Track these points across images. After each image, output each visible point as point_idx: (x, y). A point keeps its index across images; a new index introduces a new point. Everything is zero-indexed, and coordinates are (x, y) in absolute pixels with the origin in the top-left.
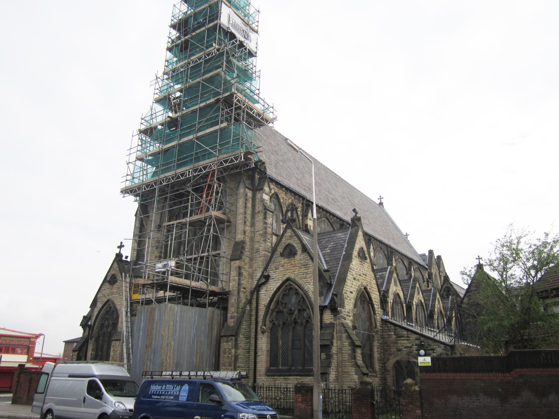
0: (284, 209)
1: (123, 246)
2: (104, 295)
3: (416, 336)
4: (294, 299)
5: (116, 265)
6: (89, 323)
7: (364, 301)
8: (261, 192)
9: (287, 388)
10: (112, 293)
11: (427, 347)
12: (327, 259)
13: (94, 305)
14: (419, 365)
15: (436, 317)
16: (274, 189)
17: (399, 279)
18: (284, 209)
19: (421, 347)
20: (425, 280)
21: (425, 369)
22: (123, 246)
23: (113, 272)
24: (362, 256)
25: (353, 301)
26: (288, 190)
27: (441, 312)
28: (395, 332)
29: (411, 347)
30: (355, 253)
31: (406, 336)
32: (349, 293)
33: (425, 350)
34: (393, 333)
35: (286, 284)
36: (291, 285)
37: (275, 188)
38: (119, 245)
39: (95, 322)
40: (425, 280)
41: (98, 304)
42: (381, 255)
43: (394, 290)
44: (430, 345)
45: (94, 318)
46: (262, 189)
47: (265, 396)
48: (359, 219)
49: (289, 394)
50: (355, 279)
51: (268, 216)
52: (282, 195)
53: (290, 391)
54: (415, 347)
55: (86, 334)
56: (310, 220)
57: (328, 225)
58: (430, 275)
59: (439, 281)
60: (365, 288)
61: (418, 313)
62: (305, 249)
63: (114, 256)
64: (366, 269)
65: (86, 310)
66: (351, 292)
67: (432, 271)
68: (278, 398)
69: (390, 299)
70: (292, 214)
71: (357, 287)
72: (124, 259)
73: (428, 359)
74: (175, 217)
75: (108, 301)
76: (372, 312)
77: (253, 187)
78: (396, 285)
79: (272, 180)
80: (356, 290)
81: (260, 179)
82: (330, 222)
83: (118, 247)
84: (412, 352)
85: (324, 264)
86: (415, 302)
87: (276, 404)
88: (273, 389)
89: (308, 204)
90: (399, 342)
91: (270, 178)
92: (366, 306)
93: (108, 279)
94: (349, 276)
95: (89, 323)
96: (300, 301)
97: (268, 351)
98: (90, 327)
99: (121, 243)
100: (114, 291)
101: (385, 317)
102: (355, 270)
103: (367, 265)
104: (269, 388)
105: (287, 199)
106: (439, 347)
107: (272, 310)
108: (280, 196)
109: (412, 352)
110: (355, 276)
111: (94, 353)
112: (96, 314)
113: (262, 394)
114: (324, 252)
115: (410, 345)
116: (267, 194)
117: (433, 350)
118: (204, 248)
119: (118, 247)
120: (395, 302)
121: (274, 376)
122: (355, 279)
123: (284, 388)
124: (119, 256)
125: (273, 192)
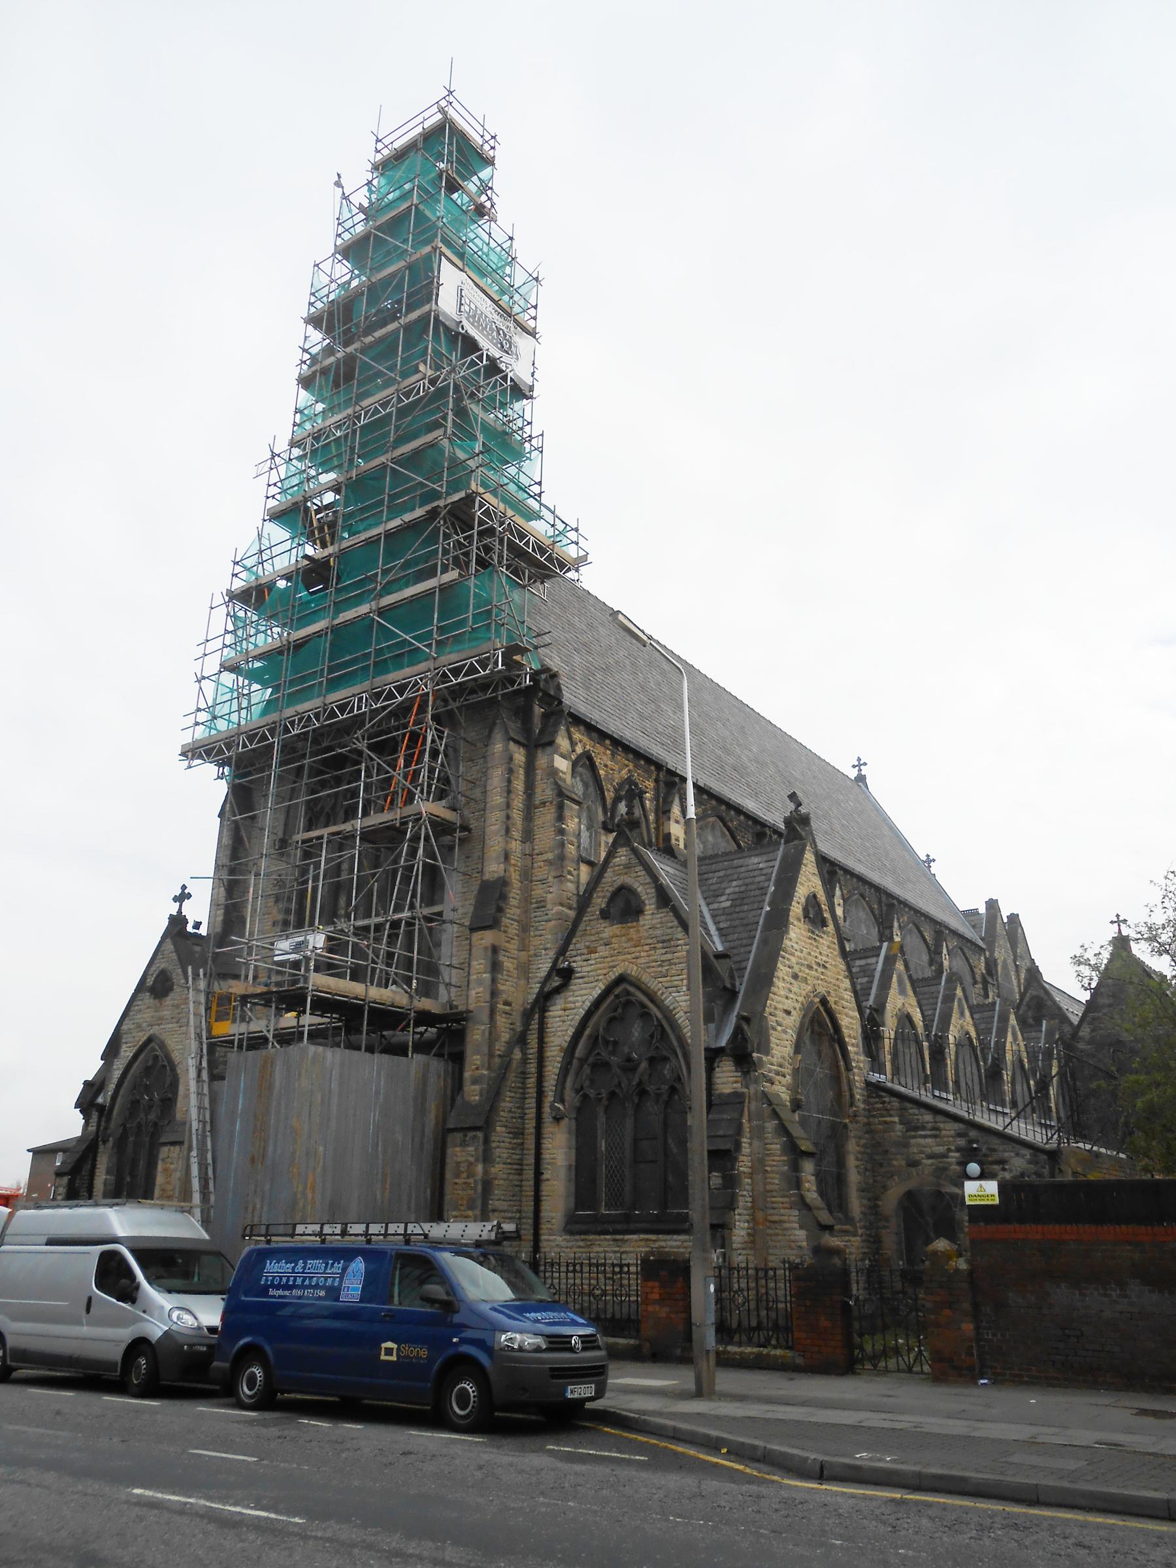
0: (610, 796)
1: (189, 896)
2: (139, 1026)
3: (962, 1126)
5: (169, 946)
6: (100, 1100)
7: (820, 1034)
8: (549, 750)
9: (621, 1266)
10: (161, 1018)
11: (985, 1155)
12: (722, 925)
13: (111, 1052)
14: (968, 1202)
15: (1006, 1076)
16: (584, 743)
17: (910, 977)
18: (610, 796)
19: (970, 1154)
20: (979, 978)
21: (981, 1213)
22: (189, 896)
23: (161, 965)
24: (815, 917)
25: (791, 1035)
26: (619, 745)
27: (1021, 1061)
29: (945, 1156)
30: (796, 909)
32: (781, 1014)
33: (980, 1163)
34: (896, 1119)
35: (617, 991)
36: (628, 993)
37: (585, 739)
38: (178, 892)
39: (114, 1098)
40: (979, 978)
42: (862, 914)
43: (899, 1005)
44: (994, 1150)
45: (111, 1087)
46: (551, 743)
48: (805, 820)
50: (795, 976)
51: (567, 813)
52: (603, 758)
53: (628, 1272)
55: (92, 1128)
56: (677, 822)
57: (723, 835)
59: (1015, 982)
60: (824, 1002)
62: (664, 899)
63: (165, 923)
64: (825, 950)
65: (91, 1067)
66: (788, 1013)
67: (996, 954)
69: (889, 1030)
70: (630, 807)
71: (800, 999)
72: (190, 928)
73: (991, 1187)
75: (150, 1040)
77: (528, 738)
78: (903, 992)
79: (577, 720)
80: (798, 1006)
81: (546, 716)
82: (729, 829)
83: (175, 899)
84: (945, 1169)
85: (716, 939)
86: (953, 1035)
88: (586, 1269)
89: (671, 782)
90: (913, 1141)
91: (571, 715)
92: (825, 1048)
93: (150, 982)
94: (782, 971)
95: (100, 1100)
98: (101, 1109)
99: (184, 887)
100: (166, 1013)
101: (876, 1077)
102: (797, 953)
103: (827, 943)
104: (574, 1267)
105: (616, 767)
107: (580, 1059)
108: (597, 761)
109: (945, 1169)
110: (796, 969)
111: (111, 1178)
112: (117, 1074)
114: (715, 906)
116: (563, 756)
117: (1002, 1162)
118: (402, 897)
119: (175, 899)
120: (899, 1037)
121: (586, 1233)
124: (177, 921)
125: (579, 749)
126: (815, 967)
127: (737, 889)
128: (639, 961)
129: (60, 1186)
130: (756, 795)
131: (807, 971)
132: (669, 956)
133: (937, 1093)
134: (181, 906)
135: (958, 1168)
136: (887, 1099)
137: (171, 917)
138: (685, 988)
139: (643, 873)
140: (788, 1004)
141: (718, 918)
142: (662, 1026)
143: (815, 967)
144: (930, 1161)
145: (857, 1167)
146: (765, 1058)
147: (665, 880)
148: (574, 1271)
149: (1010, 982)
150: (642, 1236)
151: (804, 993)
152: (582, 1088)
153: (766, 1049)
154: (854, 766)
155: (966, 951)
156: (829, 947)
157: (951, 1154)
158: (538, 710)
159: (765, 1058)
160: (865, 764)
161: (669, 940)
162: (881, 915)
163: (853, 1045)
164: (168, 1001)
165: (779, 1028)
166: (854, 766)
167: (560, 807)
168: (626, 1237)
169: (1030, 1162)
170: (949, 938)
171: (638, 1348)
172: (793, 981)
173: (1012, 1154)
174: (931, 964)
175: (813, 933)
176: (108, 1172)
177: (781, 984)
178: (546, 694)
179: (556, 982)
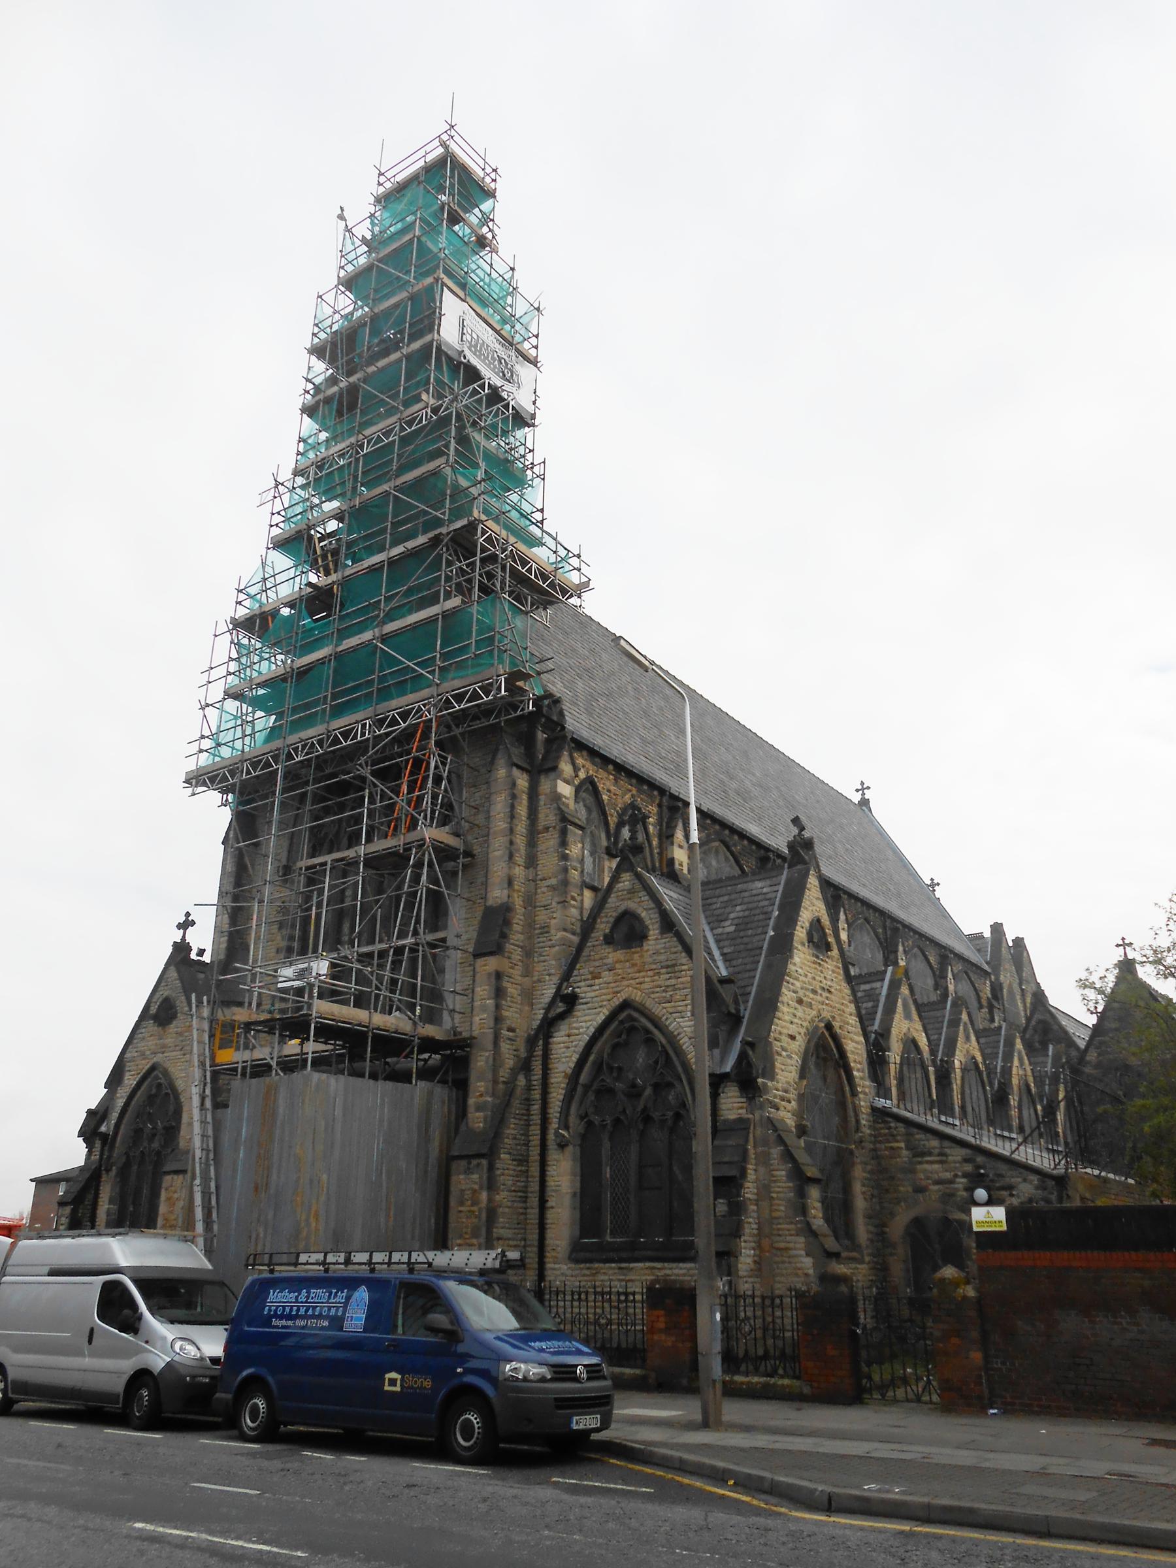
0: (613, 821)
1: (193, 923)
2: (143, 1054)
3: (968, 1151)
4: (641, 1058)
5: (173, 974)
6: (103, 1129)
8: (552, 775)
10: (164, 1046)
11: (992, 1181)
12: (726, 950)
13: (115, 1079)
14: (975, 1229)
15: (1013, 1101)
16: (587, 768)
17: (915, 1001)
18: (613, 821)
19: (977, 1180)
20: (984, 1003)
21: (988, 1239)
22: (193, 923)
23: (165, 992)
24: (819, 941)
25: (797, 1060)
26: (622, 770)
27: (1028, 1086)
28: (907, 1142)
29: (951, 1182)
30: (800, 933)
31: (936, 1151)
32: (785, 1039)
34: (902, 1145)
35: (622, 1016)
38: (182, 919)
40: (984, 1003)
41: (127, 1076)
43: (905, 1030)
44: (1001, 1176)
46: (554, 768)
47: (568, 1315)
48: (808, 845)
49: (631, 1311)
50: (800, 1001)
52: (606, 782)
53: (634, 1301)
54: (962, 1182)
55: (96, 1157)
56: (680, 847)
57: (727, 859)
58: (996, 989)
60: (829, 1027)
61: (967, 1091)
62: (668, 924)
63: (169, 950)
65: (95, 1095)
66: (793, 1038)
67: (1002, 978)
68: (603, 1321)
69: (894, 1056)
70: (633, 832)
71: (805, 1024)
72: (193, 956)
73: (998, 1214)
74: (326, 846)
75: (153, 1068)
76: (847, 1088)
78: (908, 1016)
79: (580, 746)
80: (803, 1031)
81: (548, 742)
83: (179, 926)
85: (720, 964)
87: (599, 1336)
88: (591, 1298)
89: (674, 807)
91: (574, 740)
92: (831, 1074)
93: (153, 1009)
94: (787, 995)
95: (103, 1129)
96: (656, 1062)
97: (574, 1194)
98: (104, 1137)
99: (188, 914)
100: (169, 1041)
101: (882, 1102)
102: (801, 978)
103: (831, 967)
104: (579, 1295)
105: (619, 792)
106: (1025, 1180)
108: (600, 786)
110: (801, 994)
111: (114, 1207)
112: (120, 1103)
113: (561, 1310)
114: (719, 931)
115: (948, 1175)
116: (567, 782)
117: (1010, 1188)
118: (405, 923)
119: (179, 926)
120: (905, 1061)
121: (591, 1261)
122: (800, 1001)
123: (619, 1294)
124: (181, 949)
126: (820, 991)
127: (741, 914)
128: (643, 986)
129: (62, 1215)
130: (759, 820)
131: (812, 996)
132: (673, 981)
133: (943, 1118)
134: (184, 933)
135: (965, 1194)
136: (892, 1125)
137: (175, 944)
138: (689, 1014)
139: (647, 898)
140: (793, 1029)
141: (722, 944)
142: (667, 1054)
143: (820, 991)
144: (936, 1187)
145: (863, 1193)
146: (770, 1084)
147: (670, 905)
148: (580, 1300)
149: (1016, 1005)
150: (648, 1264)
151: (809, 1018)
152: (586, 1115)
153: (770, 1073)
154: (857, 790)
155: (971, 975)
156: (833, 972)
157: (958, 1180)
158: (541, 736)
159: (770, 1084)
160: (868, 788)
161: (674, 965)
162: (886, 940)
163: (858, 1070)
164: (173, 1028)
165: (784, 1053)
166: (857, 790)
167: (564, 833)
168: (632, 1265)
169: (1037, 1188)
170: (954, 963)
171: (644, 1378)
172: (798, 1006)
173: (1019, 1180)
174: (936, 988)
175: (817, 957)
176: (110, 1202)
177: (785, 1009)
178: (549, 719)
179: (561, 1007)
